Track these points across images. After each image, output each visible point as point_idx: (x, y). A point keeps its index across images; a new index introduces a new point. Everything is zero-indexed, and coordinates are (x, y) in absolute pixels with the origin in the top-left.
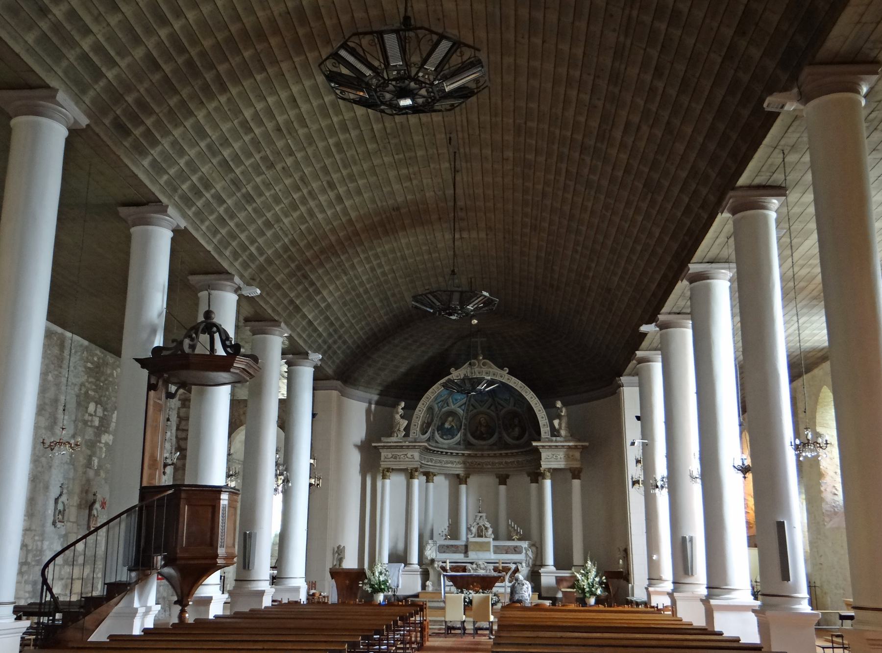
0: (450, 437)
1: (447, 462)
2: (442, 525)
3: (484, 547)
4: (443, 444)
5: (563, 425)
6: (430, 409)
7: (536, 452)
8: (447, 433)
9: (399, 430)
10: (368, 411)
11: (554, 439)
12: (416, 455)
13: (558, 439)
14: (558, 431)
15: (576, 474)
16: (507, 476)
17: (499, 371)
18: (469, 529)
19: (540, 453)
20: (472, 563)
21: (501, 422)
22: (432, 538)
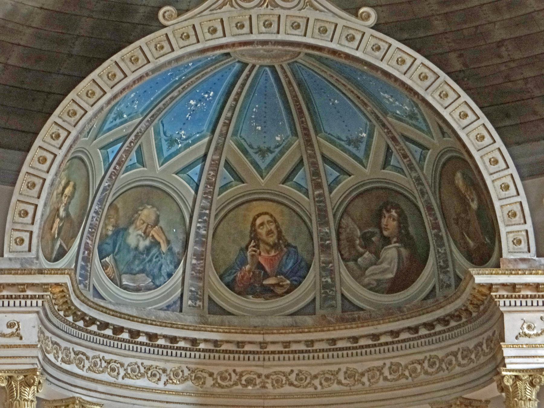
0: (145, 280)
1: (135, 372)
6: (78, 161)
7: (484, 313)
8: (143, 267)
12: (29, 324)
17: (345, 20)
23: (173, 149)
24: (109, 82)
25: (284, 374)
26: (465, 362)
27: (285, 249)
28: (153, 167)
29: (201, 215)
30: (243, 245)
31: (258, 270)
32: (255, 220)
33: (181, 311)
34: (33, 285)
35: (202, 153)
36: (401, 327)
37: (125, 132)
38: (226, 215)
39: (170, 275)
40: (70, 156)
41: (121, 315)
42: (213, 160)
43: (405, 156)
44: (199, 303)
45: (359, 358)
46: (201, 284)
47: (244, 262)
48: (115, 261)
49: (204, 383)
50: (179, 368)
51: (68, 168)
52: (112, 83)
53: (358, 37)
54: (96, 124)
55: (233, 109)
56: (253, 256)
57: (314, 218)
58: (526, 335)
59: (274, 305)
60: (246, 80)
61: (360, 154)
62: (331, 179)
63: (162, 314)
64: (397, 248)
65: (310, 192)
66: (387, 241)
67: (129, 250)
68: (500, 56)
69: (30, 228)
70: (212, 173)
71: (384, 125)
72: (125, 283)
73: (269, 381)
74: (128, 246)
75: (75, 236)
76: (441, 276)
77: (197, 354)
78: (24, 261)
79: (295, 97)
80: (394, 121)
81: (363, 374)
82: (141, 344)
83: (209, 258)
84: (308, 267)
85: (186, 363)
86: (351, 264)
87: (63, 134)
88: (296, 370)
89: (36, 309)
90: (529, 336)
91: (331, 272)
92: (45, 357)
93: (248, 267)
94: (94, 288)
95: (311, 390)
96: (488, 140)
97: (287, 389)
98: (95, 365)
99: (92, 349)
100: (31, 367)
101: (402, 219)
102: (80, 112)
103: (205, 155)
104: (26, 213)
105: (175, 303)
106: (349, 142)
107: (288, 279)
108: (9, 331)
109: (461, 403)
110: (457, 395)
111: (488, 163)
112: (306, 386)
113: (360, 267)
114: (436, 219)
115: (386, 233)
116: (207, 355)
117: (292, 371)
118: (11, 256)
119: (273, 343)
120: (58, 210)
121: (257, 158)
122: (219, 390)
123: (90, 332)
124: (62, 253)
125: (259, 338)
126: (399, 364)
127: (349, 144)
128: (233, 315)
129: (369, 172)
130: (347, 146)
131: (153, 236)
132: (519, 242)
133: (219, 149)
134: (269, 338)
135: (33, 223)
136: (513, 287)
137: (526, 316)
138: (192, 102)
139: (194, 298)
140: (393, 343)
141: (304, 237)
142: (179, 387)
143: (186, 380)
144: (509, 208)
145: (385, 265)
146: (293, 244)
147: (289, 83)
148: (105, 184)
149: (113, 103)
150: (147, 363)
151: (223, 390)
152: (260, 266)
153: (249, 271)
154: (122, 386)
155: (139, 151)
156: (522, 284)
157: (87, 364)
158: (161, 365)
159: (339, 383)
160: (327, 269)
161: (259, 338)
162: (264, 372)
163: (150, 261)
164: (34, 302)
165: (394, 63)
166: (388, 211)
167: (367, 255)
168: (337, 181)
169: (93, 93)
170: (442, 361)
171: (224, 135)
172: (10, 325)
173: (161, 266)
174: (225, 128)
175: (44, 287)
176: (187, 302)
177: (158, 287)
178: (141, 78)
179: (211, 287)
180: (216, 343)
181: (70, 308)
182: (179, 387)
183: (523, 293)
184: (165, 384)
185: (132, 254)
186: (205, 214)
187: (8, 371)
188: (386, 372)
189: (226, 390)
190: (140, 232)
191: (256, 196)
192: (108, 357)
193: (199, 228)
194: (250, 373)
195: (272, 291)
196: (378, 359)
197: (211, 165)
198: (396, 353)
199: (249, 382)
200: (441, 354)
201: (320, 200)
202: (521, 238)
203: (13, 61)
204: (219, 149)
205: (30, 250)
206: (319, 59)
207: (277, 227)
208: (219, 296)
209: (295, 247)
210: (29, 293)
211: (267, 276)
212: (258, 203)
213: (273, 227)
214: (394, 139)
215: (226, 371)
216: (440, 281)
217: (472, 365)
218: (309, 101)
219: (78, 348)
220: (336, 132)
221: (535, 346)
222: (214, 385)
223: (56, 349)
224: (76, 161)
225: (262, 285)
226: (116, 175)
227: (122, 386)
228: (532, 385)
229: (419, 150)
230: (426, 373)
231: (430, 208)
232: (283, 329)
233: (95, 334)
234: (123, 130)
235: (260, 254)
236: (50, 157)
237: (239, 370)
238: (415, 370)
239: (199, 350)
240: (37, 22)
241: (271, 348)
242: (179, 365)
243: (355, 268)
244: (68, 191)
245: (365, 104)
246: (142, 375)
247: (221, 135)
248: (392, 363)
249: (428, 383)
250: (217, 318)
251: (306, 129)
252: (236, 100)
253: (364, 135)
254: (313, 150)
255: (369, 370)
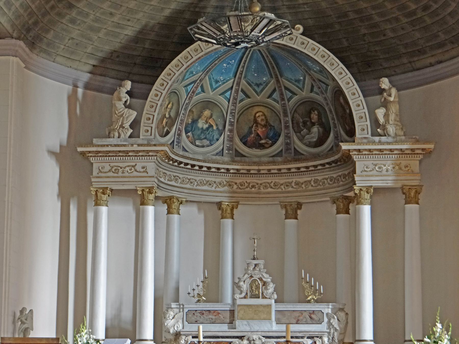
0: (206, 142)
1: (202, 183)
2: (192, 278)
3: (261, 313)
4: (195, 153)
5: (392, 117)
6: (174, 93)
7: (347, 160)
9: (122, 126)
10: (72, 98)
11: (377, 139)
12: (151, 167)
13: (383, 139)
14: (384, 128)
15: (411, 195)
16: (299, 205)
18: (236, 285)
19: (354, 163)
20: (241, 338)
21: (289, 119)
22: (177, 300)
23: (218, 85)
24: (185, 60)
25: (268, 183)
26: (344, 180)
27: (269, 127)
28: (209, 93)
29: (231, 113)
30: (251, 126)
31: (257, 136)
32: (256, 114)
33: (223, 156)
34: (152, 151)
35: (231, 86)
36: (318, 164)
37: (195, 79)
38: (243, 112)
39: (218, 140)
40: (169, 92)
41: (194, 160)
42: (236, 89)
43: (319, 88)
44: (231, 152)
45: (301, 176)
46: (232, 143)
47: (251, 133)
48: (193, 134)
49: (233, 187)
50: (222, 181)
51: (169, 97)
52: (186, 61)
53: (295, 38)
54: (181, 78)
55: (243, 67)
56: (255, 130)
57: (281, 113)
58: (365, 171)
59: (265, 152)
60: (248, 55)
61: (301, 86)
62: (288, 97)
63: (214, 157)
64: (318, 127)
65: (280, 102)
66: (313, 124)
67: (199, 129)
68: (364, 41)
69: (151, 125)
70: (235, 94)
71: (310, 75)
72: (197, 143)
73: (262, 186)
74: (199, 128)
75: (173, 125)
76: (336, 141)
77: (230, 175)
78: (149, 140)
79: (270, 62)
80: (313, 73)
81: (302, 184)
82: (204, 171)
83: (235, 131)
84: (279, 136)
85: (225, 178)
86: (298, 134)
87: (165, 84)
88: (274, 181)
89: (154, 161)
90: (367, 171)
91: (289, 138)
92: (159, 180)
93: (253, 135)
94: (183, 147)
95: (280, 190)
96: (351, 84)
97: (270, 190)
98: (183, 181)
99: (182, 174)
100: (152, 186)
101: (319, 115)
102: (173, 74)
103: (232, 87)
104: (149, 119)
105: (220, 152)
106: (296, 81)
107: (271, 140)
108: (142, 170)
109: (343, 198)
110: (341, 194)
111: (351, 95)
112: (278, 189)
113: (302, 136)
114: (333, 116)
115: (313, 121)
116: (234, 175)
117: (272, 182)
118: (143, 137)
119: (263, 170)
120: (165, 115)
121: (256, 88)
122: (240, 190)
123: (180, 167)
124: (168, 133)
125: (256, 168)
126: (318, 180)
127: (296, 82)
128: (245, 156)
129: (305, 94)
130: (295, 83)
131: (210, 123)
132: (364, 130)
133: (238, 84)
134: (261, 168)
135: (152, 123)
136: (359, 150)
137: (366, 163)
138: (224, 65)
139: (229, 149)
140: (315, 170)
141: (277, 122)
142: (222, 189)
143: (225, 186)
144: (360, 115)
145: (312, 135)
146: (273, 125)
147: (267, 56)
148: (187, 102)
149: (187, 69)
150: (207, 179)
151: (242, 190)
152: (258, 135)
153: (253, 137)
154: (196, 190)
155: (202, 87)
156: (363, 149)
157: (180, 181)
158: (214, 180)
159: (292, 187)
160: (288, 137)
161: (256, 168)
162: (260, 182)
163: (209, 134)
164: (153, 157)
165: (310, 50)
166: (314, 111)
167: (305, 130)
168: (291, 98)
169: (178, 66)
170: (335, 179)
171: (240, 78)
172: (143, 168)
173: (214, 136)
174: (240, 75)
175: (157, 151)
176: (226, 152)
177: (212, 145)
178: (199, 58)
179: (236, 144)
180: (237, 170)
181: (169, 158)
182: (222, 189)
183: (364, 153)
184: (215, 188)
185: (200, 131)
186: (233, 113)
187: (142, 187)
188: (312, 183)
189: (243, 190)
190: (204, 121)
191: (256, 104)
192: (189, 177)
193: (230, 118)
194: (253, 182)
195: (263, 146)
196: (309, 177)
197: (235, 91)
198: (316, 175)
199: (253, 187)
200: (335, 176)
201: (284, 106)
202: (364, 128)
203: (147, 46)
204: (238, 84)
205: (151, 135)
206: (279, 47)
207: (266, 117)
208: (240, 148)
209: (274, 126)
210: (150, 154)
211: (261, 139)
212: (257, 107)
213: (263, 117)
214: (314, 80)
215: (243, 182)
216: (335, 143)
217: (347, 182)
218: (277, 64)
219: (175, 174)
220: (290, 76)
221: (369, 176)
222: (237, 188)
223: (165, 176)
224: (173, 94)
225: (259, 143)
226: (191, 98)
227: (196, 190)
228: (368, 193)
229: (325, 86)
230: (329, 184)
231: (331, 111)
232: (269, 163)
233: (183, 168)
234: (194, 78)
235: (258, 130)
236: (160, 94)
237: (248, 181)
238: (324, 183)
239: (230, 173)
240: (156, 29)
241: (262, 172)
242: (221, 180)
243: (300, 136)
244: (169, 106)
245: (301, 66)
246: (205, 185)
247: (239, 78)
248: (315, 179)
249: (329, 188)
250: (238, 159)
251: (276, 75)
252: (244, 63)
253: (302, 78)
254: (280, 84)
255: (305, 182)
